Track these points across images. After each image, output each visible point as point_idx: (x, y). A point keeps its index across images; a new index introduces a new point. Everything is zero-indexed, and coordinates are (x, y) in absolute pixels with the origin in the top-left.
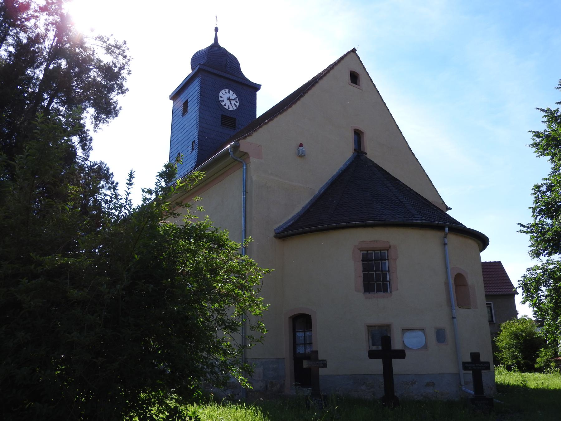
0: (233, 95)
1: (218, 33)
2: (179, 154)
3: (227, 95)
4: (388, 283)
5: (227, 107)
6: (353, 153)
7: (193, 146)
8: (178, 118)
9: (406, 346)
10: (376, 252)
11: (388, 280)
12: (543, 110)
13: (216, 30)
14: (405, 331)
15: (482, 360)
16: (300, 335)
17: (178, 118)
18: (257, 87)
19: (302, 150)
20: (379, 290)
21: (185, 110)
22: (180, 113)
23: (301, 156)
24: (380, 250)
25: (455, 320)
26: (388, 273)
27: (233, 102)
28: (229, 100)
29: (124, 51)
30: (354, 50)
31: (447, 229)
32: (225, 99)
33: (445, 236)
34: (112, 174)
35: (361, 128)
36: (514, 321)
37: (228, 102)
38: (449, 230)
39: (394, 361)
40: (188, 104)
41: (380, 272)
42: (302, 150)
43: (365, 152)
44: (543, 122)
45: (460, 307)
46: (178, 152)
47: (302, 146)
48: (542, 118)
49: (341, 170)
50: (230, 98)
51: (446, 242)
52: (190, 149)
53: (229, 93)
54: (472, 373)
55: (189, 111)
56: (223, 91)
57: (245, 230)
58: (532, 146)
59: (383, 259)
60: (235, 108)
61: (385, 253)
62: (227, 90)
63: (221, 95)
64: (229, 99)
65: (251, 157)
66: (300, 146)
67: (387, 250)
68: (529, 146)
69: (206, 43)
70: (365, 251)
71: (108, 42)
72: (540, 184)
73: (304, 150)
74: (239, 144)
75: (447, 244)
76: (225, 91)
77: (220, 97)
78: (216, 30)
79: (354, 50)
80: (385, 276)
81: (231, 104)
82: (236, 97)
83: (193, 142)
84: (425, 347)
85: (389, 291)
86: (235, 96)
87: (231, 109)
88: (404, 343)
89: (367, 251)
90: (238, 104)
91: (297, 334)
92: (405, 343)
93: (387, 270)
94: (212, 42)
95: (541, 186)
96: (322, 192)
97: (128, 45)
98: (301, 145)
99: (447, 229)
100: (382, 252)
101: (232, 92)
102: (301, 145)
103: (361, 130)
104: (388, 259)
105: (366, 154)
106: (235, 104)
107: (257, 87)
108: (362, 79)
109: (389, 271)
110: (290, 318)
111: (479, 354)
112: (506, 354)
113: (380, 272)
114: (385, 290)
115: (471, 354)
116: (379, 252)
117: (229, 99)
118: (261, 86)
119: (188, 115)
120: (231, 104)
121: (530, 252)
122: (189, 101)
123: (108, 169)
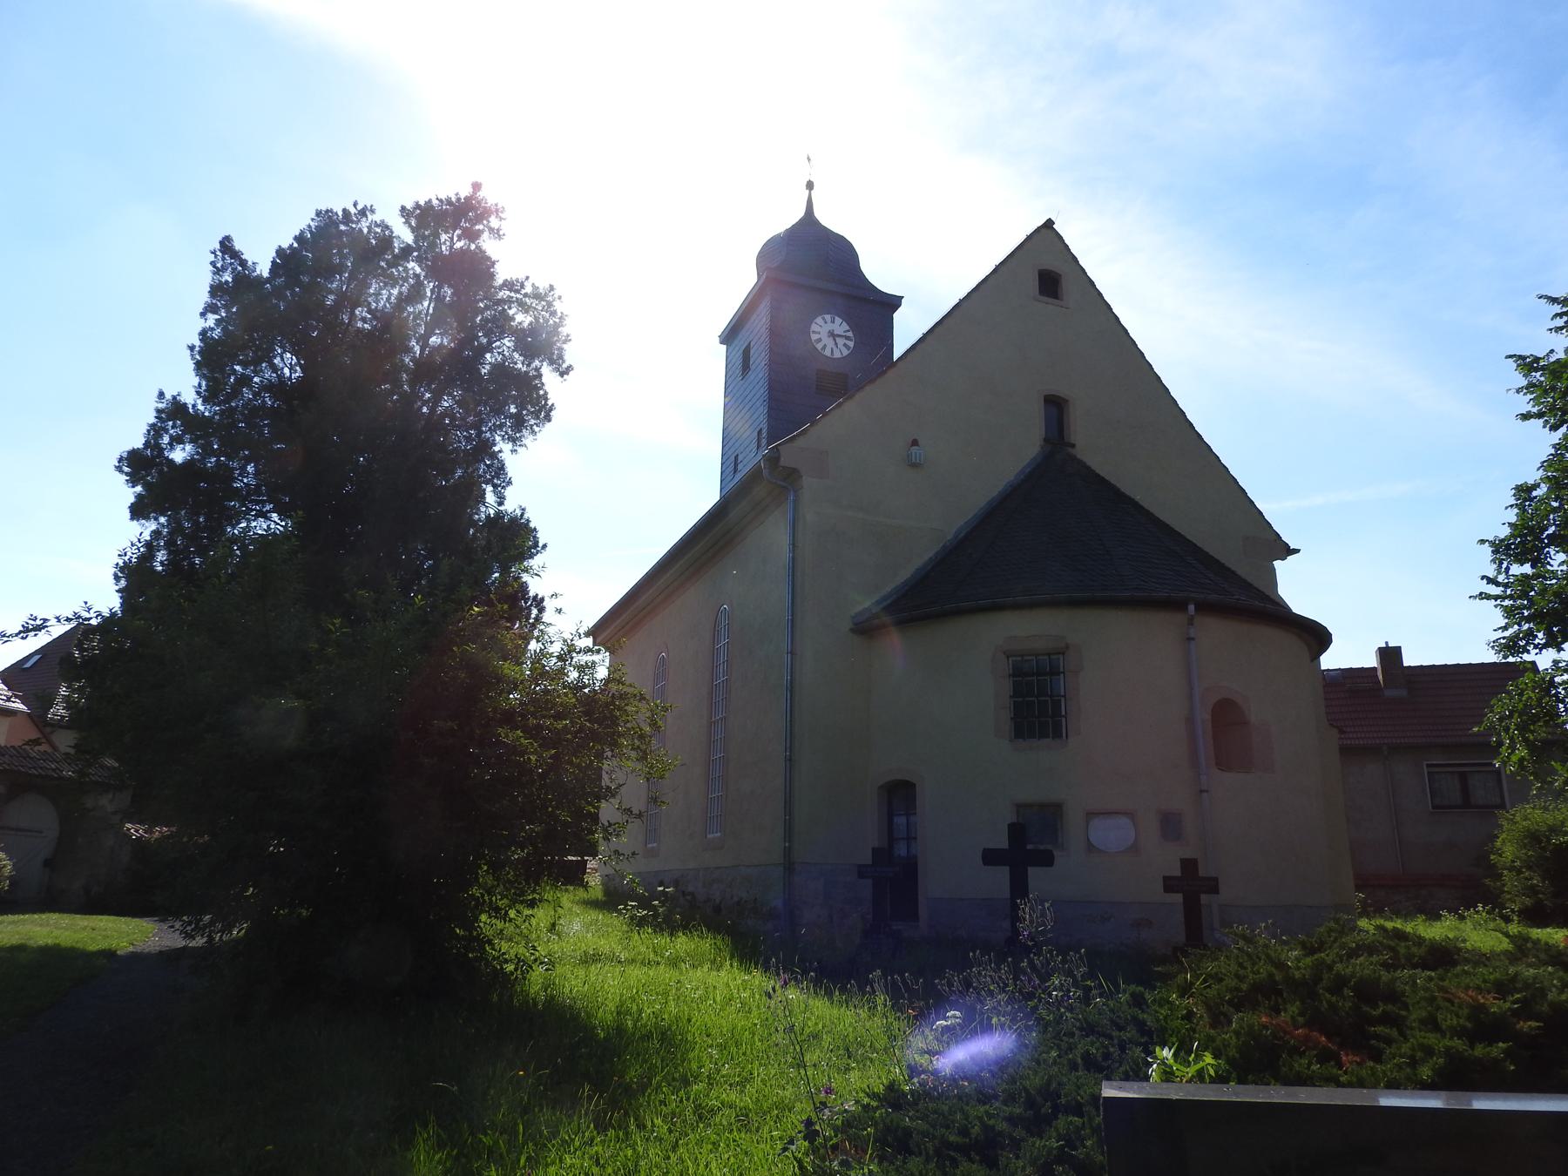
0: (840, 326)
1: (812, 192)
2: (736, 457)
3: (830, 327)
4: (1064, 720)
5: (827, 353)
6: (1042, 448)
7: (759, 441)
8: (735, 383)
9: (1094, 846)
10: (1041, 657)
11: (1063, 713)
12: (1554, 300)
13: (810, 186)
14: (1090, 815)
15: (1202, 873)
16: (900, 821)
17: (735, 383)
18: (893, 303)
19: (916, 453)
20: (1044, 735)
21: (746, 366)
22: (739, 371)
23: (914, 465)
24: (1049, 654)
25: (1205, 795)
26: (1063, 699)
27: (841, 341)
28: (831, 338)
29: (550, 304)
30: (1049, 224)
31: (1192, 608)
32: (824, 335)
33: (1191, 622)
34: (535, 529)
35: (1062, 390)
36: (1535, 806)
37: (830, 343)
38: (1196, 609)
39: (1031, 871)
40: (752, 352)
41: (1047, 698)
42: (916, 453)
43: (1073, 442)
44: (1551, 330)
45: (1222, 770)
46: (736, 454)
47: (918, 445)
48: (1552, 319)
49: (1011, 486)
50: (835, 333)
51: (1192, 635)
52: (754, 446)
53: (833, 322)
54: (1181, 900)
55: (753, 367)
56: (819, 320)
57: (792, 620)
58: (1525, 391)
59: (1055, 672)
60: (846, 352)
61: (1059, 659)
62: (828, 317)
63: (814, 327)
64: (832, 335)
65: (804, 478)
66: (912, 446)
67: (1063, 654)
68: (1518, 391)
69: (791, 216)
70: (1019, 656)
71: (523, 292)
72: (1531, 482)
73: (920, 454)
74: (780, 454)
75: (1193, 639)
76: (824, 319)
77: (814, 332)
78: (810, 186)
79: (1049, 224)
80: (1057, 705)
81: (836, 344)
82: (848, 328)
83: (760, 432)
84: (1134, 849)
85: (1064, 735)
86: (845, 326)
87: (837, 355)
88: (1088, 840)
89: (1022, 656)
90: (851, 344)
91: (895, 819)
92: (1091, 839)
93: (1062, 693)
94: (800, 213)
95: (1536, 486)
96: (962, 535)
97: (557, 293)
98: (915, 443)
99: (1192, 608)
100: (1053, 657)
101: (838, 320)
102: (915, 443)
103: (1062, 395)
104: (1064, 673)
105: (1073, 446)
106: (845, 345)
107: (893, 303)
108: (1067, 286)
109: (1065, 696)
110: (881, 787)
111: (1186, 859)
112: (1510, 882)
113: (1047, 698)
114: (1057, 734)
115: (1181, 859)
116: (1046, 657)
117: (832, 335)
118: (903, 300)
119: (751, 375)
120: (836, 344)
121: (1492, 644)
122: (752, 346)
123: (528, 521)
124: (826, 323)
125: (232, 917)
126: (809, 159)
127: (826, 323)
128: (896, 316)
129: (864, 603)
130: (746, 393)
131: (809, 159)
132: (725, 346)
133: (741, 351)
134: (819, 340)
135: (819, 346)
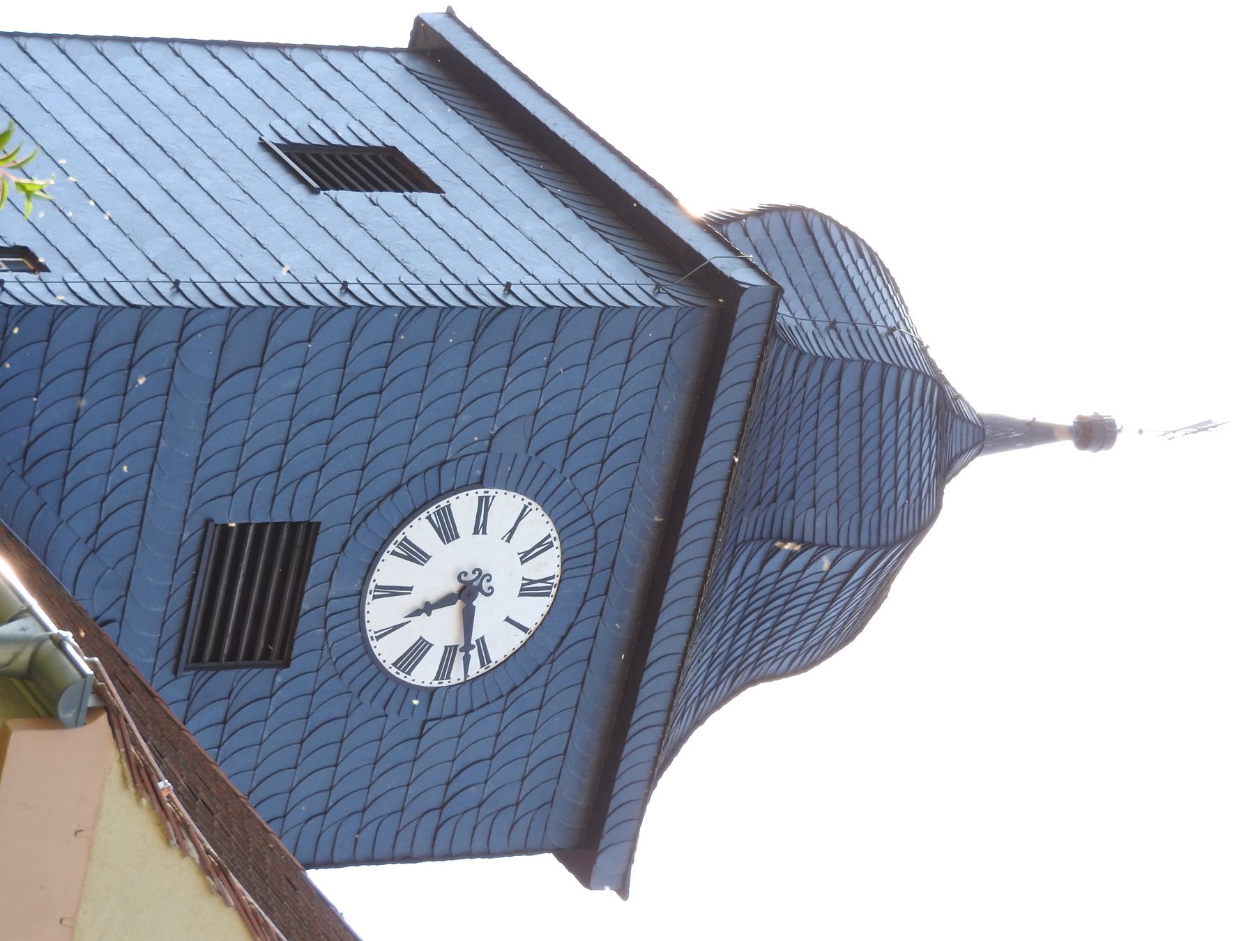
5: (390, 569)
28: (455, 587)
40: (390, 199)
50: (480, 602)
53: (529, 589)
55: (322, 203)
60: (387, 651)
62: (549, 565)
63: (506, 504)
76: (544, 546)
77: (484, 504)
81: (428, 608)
82: (497, 655)
87: (378, 613)
101: (534, 611)
106: (421, 648)
120: (428, 608)
124: (525, 557)
125: (292, 922)
126: (1202, 427)
127: (525, 557)
128: (547, 863)
129: (784, 499)
130: (199, 165)
131: (1202, 427)
132: (404, 43)
133: (392, 137)
134: (447, 531)
135: (420, 531)
